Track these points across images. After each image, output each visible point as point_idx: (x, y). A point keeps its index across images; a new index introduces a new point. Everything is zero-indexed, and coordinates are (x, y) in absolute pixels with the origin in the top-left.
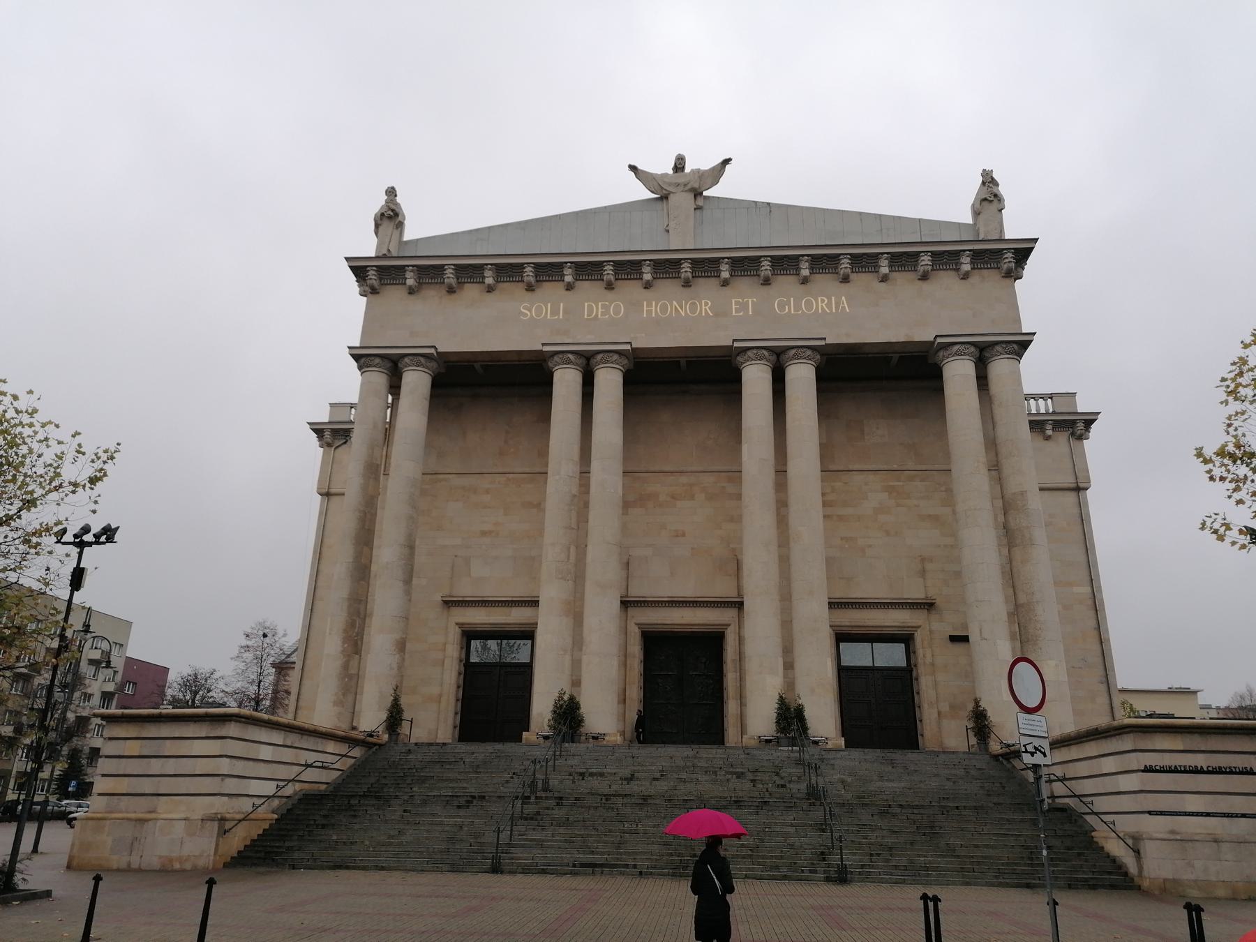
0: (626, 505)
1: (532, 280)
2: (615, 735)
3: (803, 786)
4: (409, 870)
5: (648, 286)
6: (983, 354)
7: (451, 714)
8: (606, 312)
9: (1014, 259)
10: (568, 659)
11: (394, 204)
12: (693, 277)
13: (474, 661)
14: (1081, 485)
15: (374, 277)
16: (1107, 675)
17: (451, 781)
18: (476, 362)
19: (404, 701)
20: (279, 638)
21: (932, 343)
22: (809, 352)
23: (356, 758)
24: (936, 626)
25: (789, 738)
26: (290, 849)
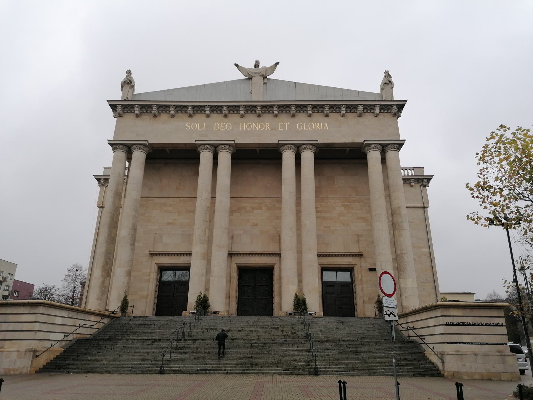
0: (232, 212)
1: (191, 112)
2: (224, 312)
3: (303, 333)
4: (122, 373)
5: (242, 116)
6: (384, 148)
7: (152, 304)
8: (224, 127)
9: (397, 108)
10: (204, 278)
11: (130, 77)
12: (262, 113)
13: (164, 280)
14: (425, 206)
16: (435, 286)
17: (148, 333)
18: (166, 148)
19: (129, 298)
20: (83, 272)
21: (363, 143)
22: (311, 146)
23: (105, 323)
24: (363, 264)
25: (299, 312)
26: (68, 364)
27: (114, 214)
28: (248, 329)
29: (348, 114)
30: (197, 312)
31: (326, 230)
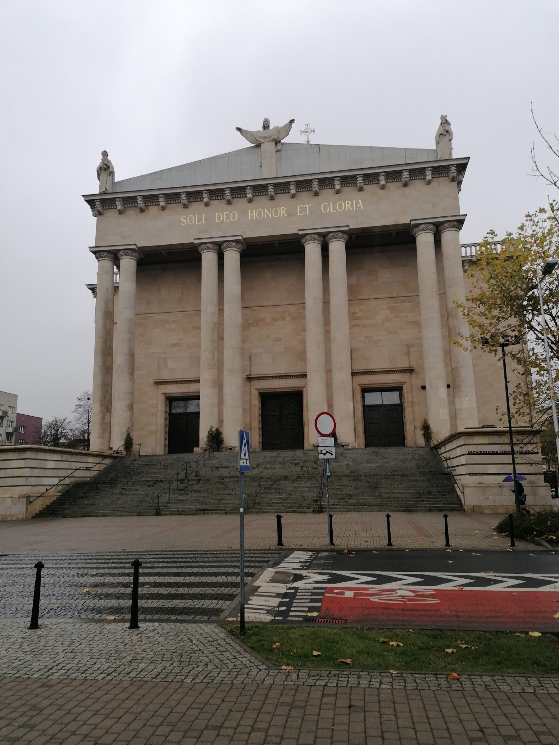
0: (246, 326)
5: (250, 201)
7: (163, 439)
9: (456, 170)
15: (98, 206)
17: (153, 473)
22: (340, 234)
26: (64, 509)
27: (106, 339)
28: (264, 466)
29: (389, 185)
30: (210, 448)
31: (367, 341)
